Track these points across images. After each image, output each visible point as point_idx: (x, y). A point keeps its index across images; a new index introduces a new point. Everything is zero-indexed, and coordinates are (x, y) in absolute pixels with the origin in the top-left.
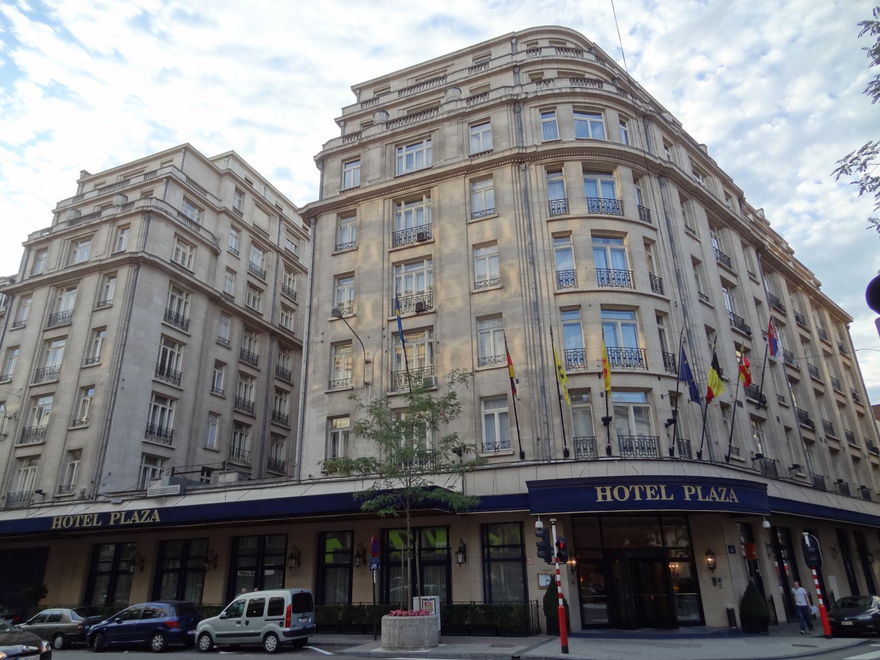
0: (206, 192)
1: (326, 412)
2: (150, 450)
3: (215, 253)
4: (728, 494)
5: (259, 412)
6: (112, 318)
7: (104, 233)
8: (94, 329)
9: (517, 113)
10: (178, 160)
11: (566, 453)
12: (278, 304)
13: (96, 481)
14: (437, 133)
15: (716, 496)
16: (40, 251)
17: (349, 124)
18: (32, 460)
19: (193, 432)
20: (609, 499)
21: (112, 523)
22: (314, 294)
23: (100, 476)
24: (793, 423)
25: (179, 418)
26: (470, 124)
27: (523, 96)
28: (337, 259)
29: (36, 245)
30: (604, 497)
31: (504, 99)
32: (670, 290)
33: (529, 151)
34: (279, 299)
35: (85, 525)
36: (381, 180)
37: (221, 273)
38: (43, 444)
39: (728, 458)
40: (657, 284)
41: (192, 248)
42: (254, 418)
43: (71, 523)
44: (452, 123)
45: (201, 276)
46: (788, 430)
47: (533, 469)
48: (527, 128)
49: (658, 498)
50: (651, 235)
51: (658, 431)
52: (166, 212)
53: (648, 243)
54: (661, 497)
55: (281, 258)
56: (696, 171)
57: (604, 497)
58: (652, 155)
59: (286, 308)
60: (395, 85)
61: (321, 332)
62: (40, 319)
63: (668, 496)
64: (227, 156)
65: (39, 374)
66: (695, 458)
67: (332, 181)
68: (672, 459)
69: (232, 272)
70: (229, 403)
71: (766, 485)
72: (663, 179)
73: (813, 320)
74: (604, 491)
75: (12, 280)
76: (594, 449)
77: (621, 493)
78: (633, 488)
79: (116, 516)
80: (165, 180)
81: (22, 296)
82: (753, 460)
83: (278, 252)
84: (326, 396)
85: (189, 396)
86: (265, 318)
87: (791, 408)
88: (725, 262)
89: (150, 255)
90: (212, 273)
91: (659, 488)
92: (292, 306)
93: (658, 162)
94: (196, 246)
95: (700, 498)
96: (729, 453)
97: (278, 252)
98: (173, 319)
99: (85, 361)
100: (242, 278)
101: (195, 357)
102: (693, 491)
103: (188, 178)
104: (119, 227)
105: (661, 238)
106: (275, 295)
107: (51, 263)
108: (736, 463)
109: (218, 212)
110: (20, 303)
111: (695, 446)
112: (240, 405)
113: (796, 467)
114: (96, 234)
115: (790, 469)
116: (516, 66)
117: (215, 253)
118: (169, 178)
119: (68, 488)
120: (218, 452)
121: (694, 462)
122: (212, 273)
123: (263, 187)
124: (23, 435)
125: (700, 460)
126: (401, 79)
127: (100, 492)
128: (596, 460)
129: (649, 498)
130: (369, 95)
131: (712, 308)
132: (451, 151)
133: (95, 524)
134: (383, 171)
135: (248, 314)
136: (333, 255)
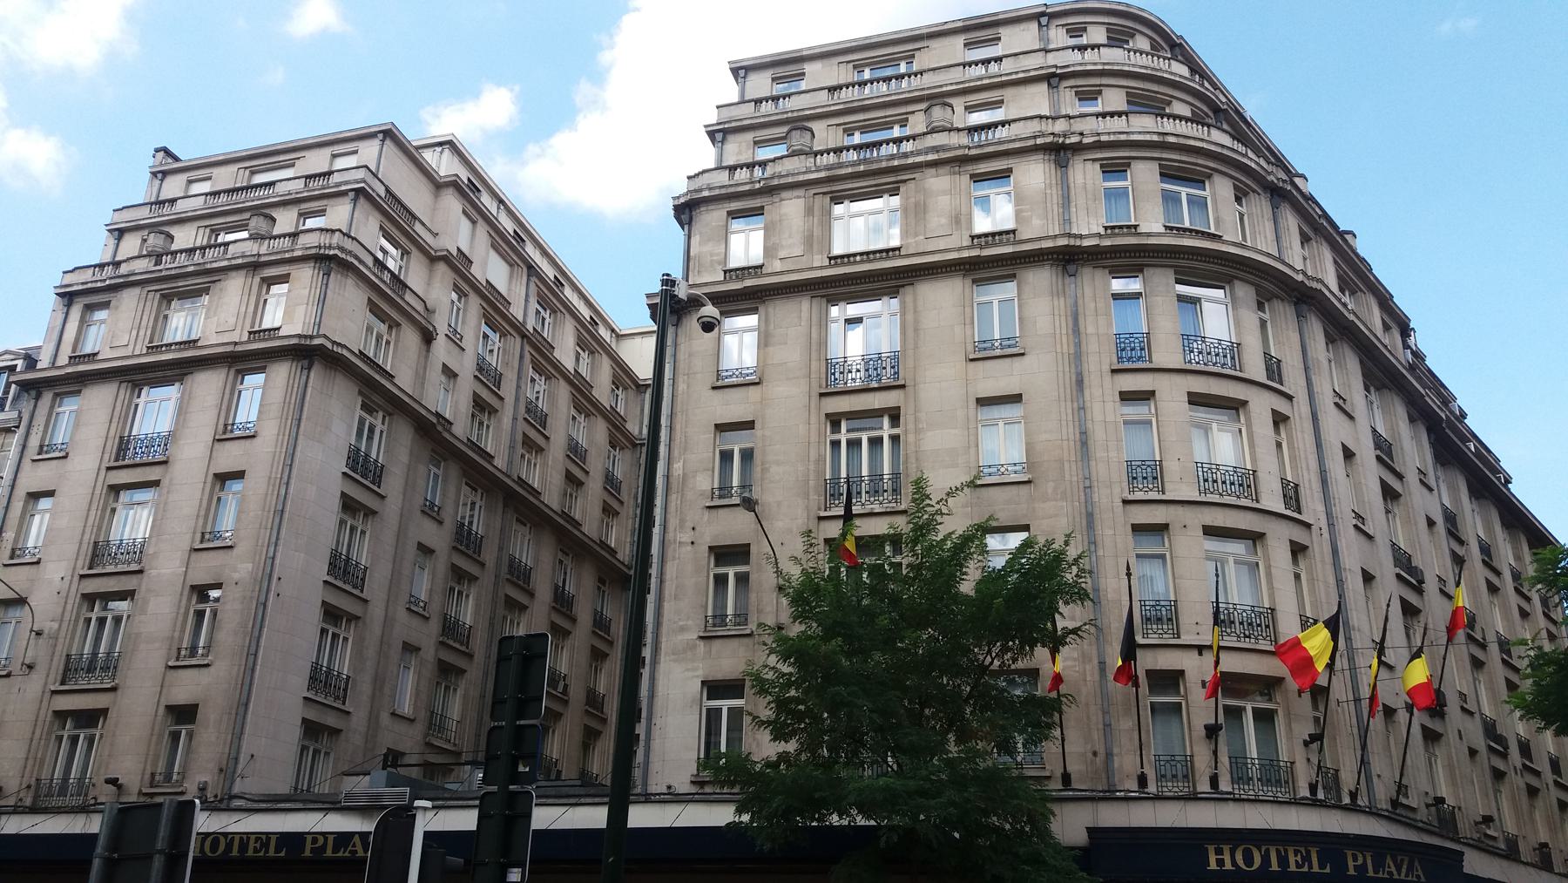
0: (415, 217)
1: (700, 672)
2: (312, 715)
3: (428, 337)
4: (1410, 869)
5: (479, 644)
6: (260, 458)
7: (234, 290)
8: (216, 476)
9: (1062, 165)
10: (369, 152)
11: (1142, 780)
12: (519, 438)
13: (228, 771)
14: (911, 185)
15: (1393, 869)
16: (90, 308)
17: (731, 138)
18: (90, 718)
19: (379, 681)
20: (1228, 866)
21: (307, 853)
22: (676, 453)
23: (237, 759)
24: (1480, 742)
25: (358, 655)
26: (972, 176)
27: (1074, 139)
28: (719, 394)
29: (83, 297)
30: (1220, 862)
31: (1039, 141)
32: (1313, 509)
33: (1086, 243)
34: (522, 426)
35: (250, 853)
36: (803, 263)
37: (435, 375)
38: (114, 689)
39: (1395, 803)
40: (1292, 495)
41: (390, 327)
42: (470, 656)
43: (222, 847)
44: (941, 170)
45: (405, 380)
46: (1473, 752)
47: (1088, 806)
48: (1078, 199)
49: (1305, 869)
50: (1282, 406)
51: (1291, 751)
52: (357, 258)
53: (1279, 420)
54: (1311, 867)
55: (527, 348)
56: (1344, 284)
57: (1220, 862)
58: (1284, 263)
59: (528, 443)
60: (818, 75)
61: (689, 525)
62: (101, 442)
63: (1322, 866)
64: (440, 144)
65: (98, 552)
66: (1347, 800)
67: (708, 248)
68: (1313, 803)
69: (449, 373)
70: (434, 626)
71: (1462, 854)
72: (1305, 307)
73: (1506, 554)
74: (1219, 852)
75: (31, 361)
76: (1189, 775)
77: (1249, 859)
78: (1267, 851)
79: (315, 840)
80: (352, 194)
81: (57, 395)
82: (1428, 806)
83: (523, 336)
84: (701, 643)
85: (376, 611)
86: (498, 462)
87: (1477, 716)
88: (1385, 451)
89: (334, 343)
90: (421, 377)
91: (1308, 852)
92: (540, 441)
93: (1300, 278)
94: (398, 325)
95: (1371, 873)
96: (1398, 792)
97: (523, 336)
98: (361, 467)
99: (199, 536)
100: (467, 385)
101: (389, 536)
102: (1360, 861)
103: (388, 190)
104: (263, 280)
105: (1299, 412)
106: (515, 419)
107: (115, 334)
108: (1403, 812)
109: (433, 258)
110: (52, 407)
111: (1348, 779)
112: (450, 628)
113: (1488, 820)
114: (215, 288)
115: (1477, 823)
116: (1054, 75)
117: (428, 337)
118: (360, 192)
119: (168, 777)
120: (412, 721)
121: (1345, 808)
122: (421, 377)
123: (495, 205)
124: (67, 669)
125: (1353, 808)
126: (826, 62)
127: (236, 790)
128: (1193, 797)
129: (1293, 868)
130: (761, 84)
131: (1370, 537)
132: (937, 221)
133: (271, 853)
134: (809, 241)
135: (470, 453)
136: (714, 388)
